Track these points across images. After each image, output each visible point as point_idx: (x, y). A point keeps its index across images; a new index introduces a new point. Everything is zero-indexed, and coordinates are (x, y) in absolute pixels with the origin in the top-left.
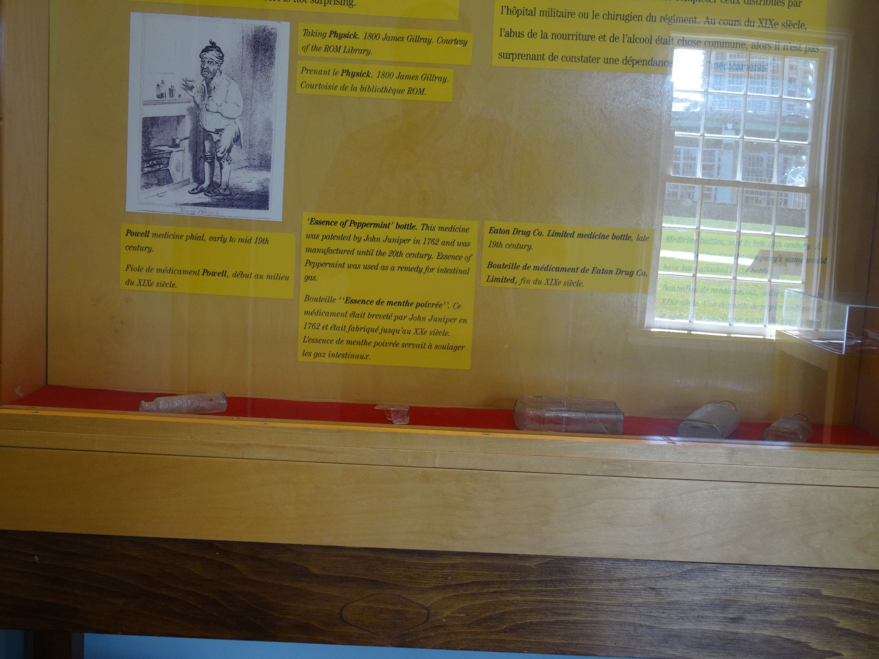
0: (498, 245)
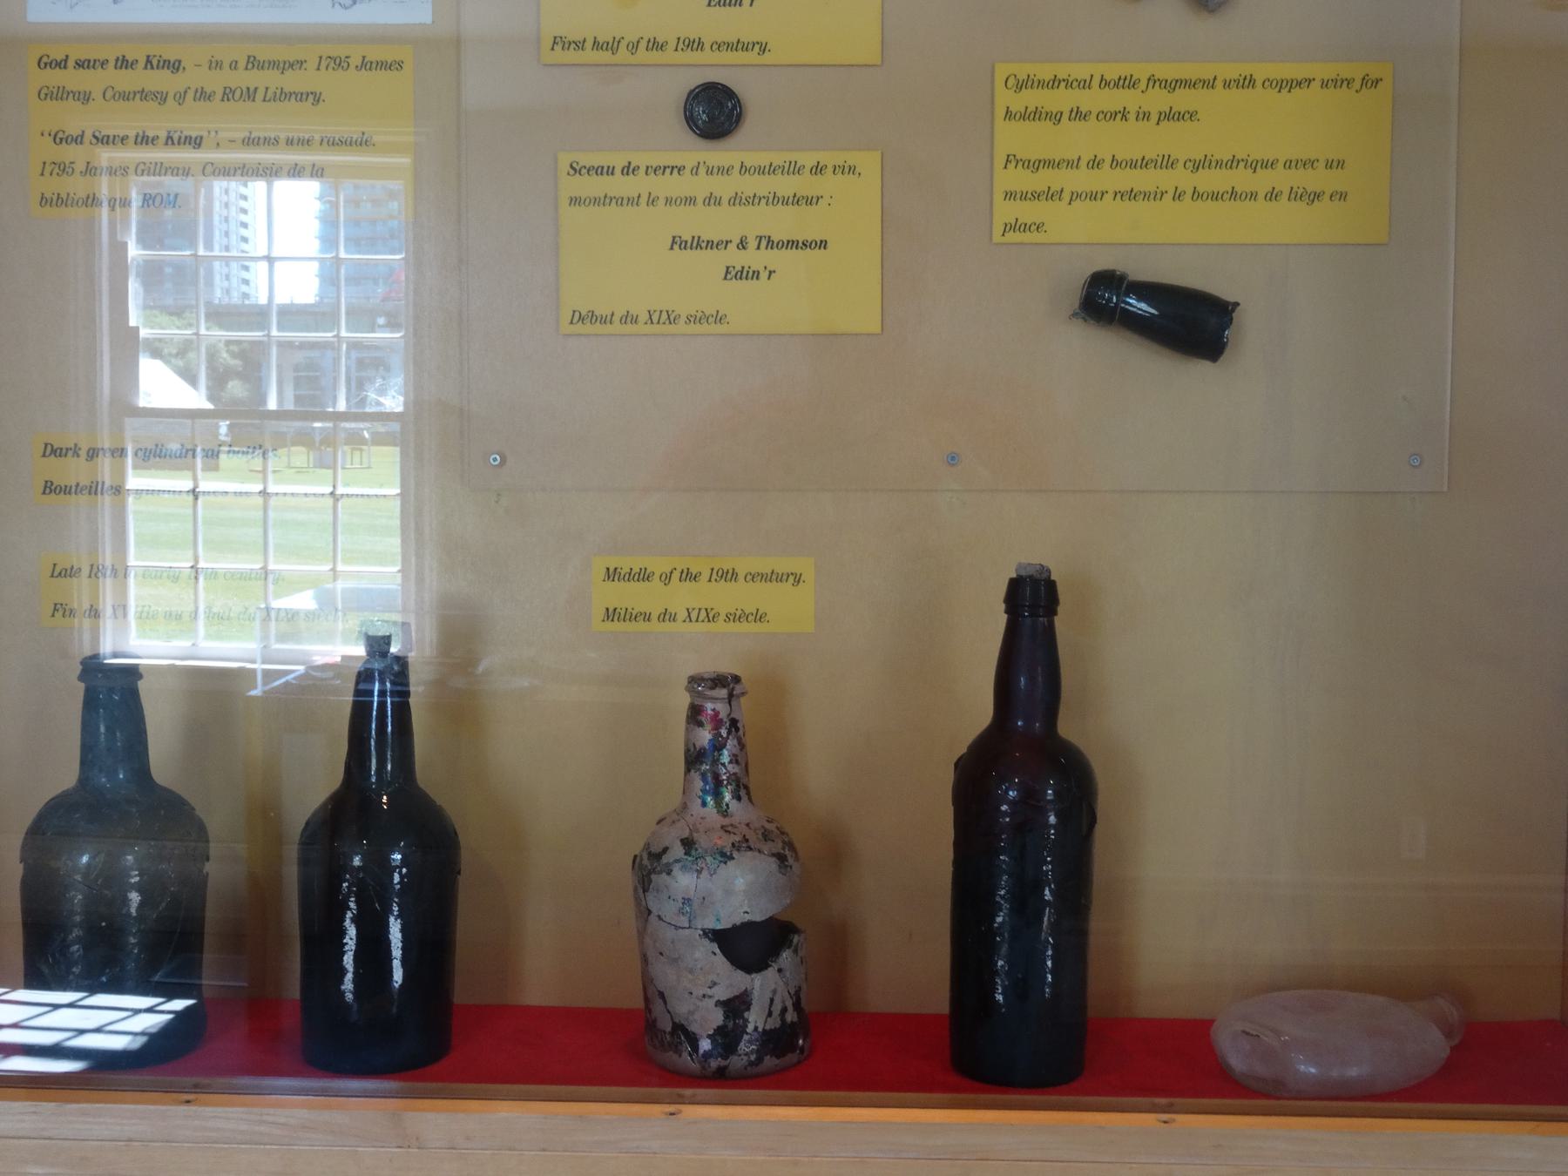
0: (59, 94)
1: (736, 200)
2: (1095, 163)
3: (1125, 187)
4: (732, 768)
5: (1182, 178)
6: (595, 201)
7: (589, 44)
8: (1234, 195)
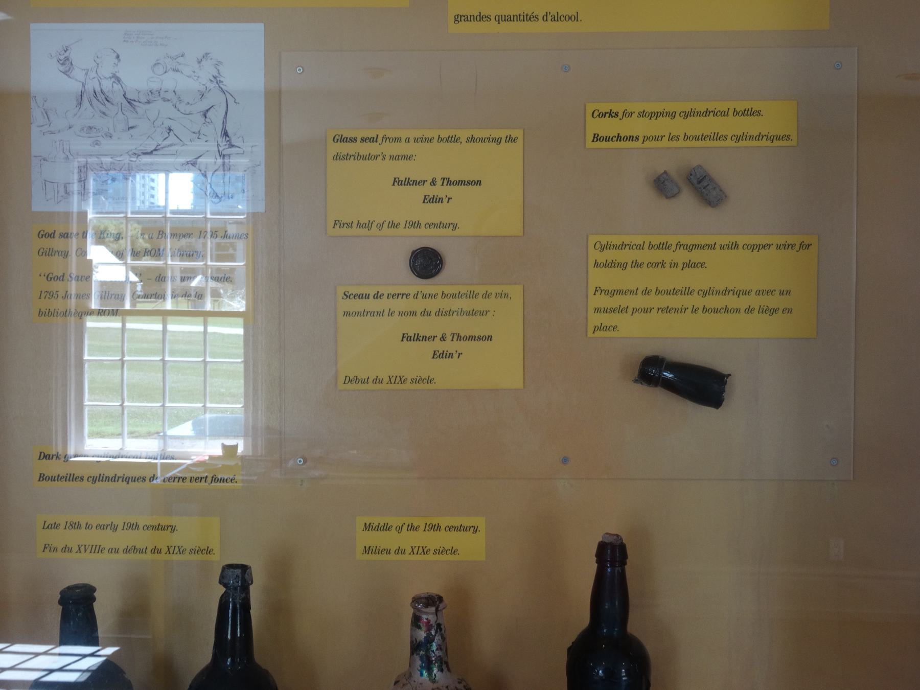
1: (439, 313)
2: (646, 292)
3: (664, 306)
4: (438, 653)
5: (697, 301)
6: (358, 314)
7: (355, 225)
8: (727, 310)
